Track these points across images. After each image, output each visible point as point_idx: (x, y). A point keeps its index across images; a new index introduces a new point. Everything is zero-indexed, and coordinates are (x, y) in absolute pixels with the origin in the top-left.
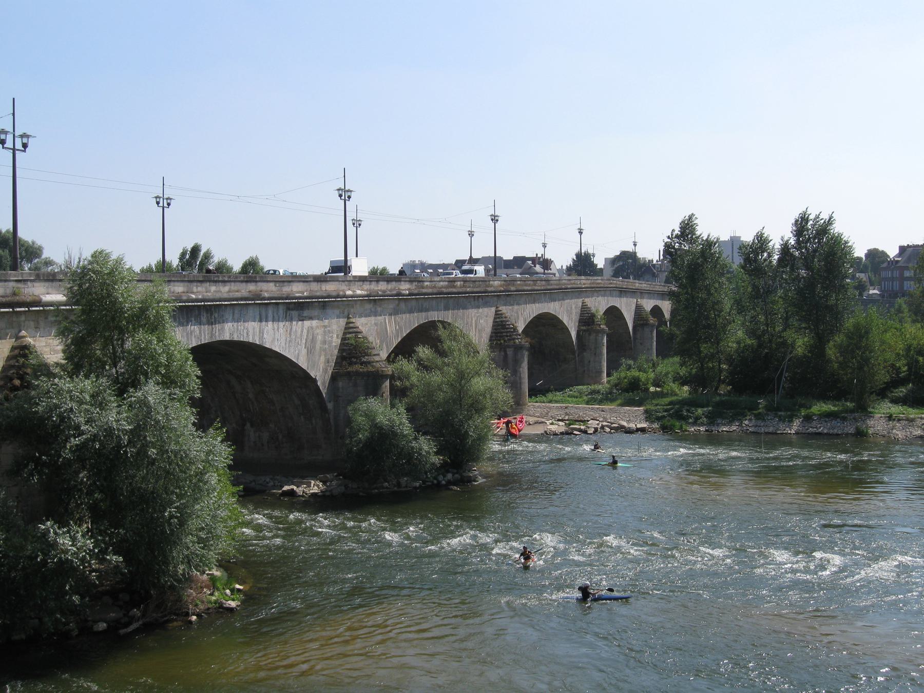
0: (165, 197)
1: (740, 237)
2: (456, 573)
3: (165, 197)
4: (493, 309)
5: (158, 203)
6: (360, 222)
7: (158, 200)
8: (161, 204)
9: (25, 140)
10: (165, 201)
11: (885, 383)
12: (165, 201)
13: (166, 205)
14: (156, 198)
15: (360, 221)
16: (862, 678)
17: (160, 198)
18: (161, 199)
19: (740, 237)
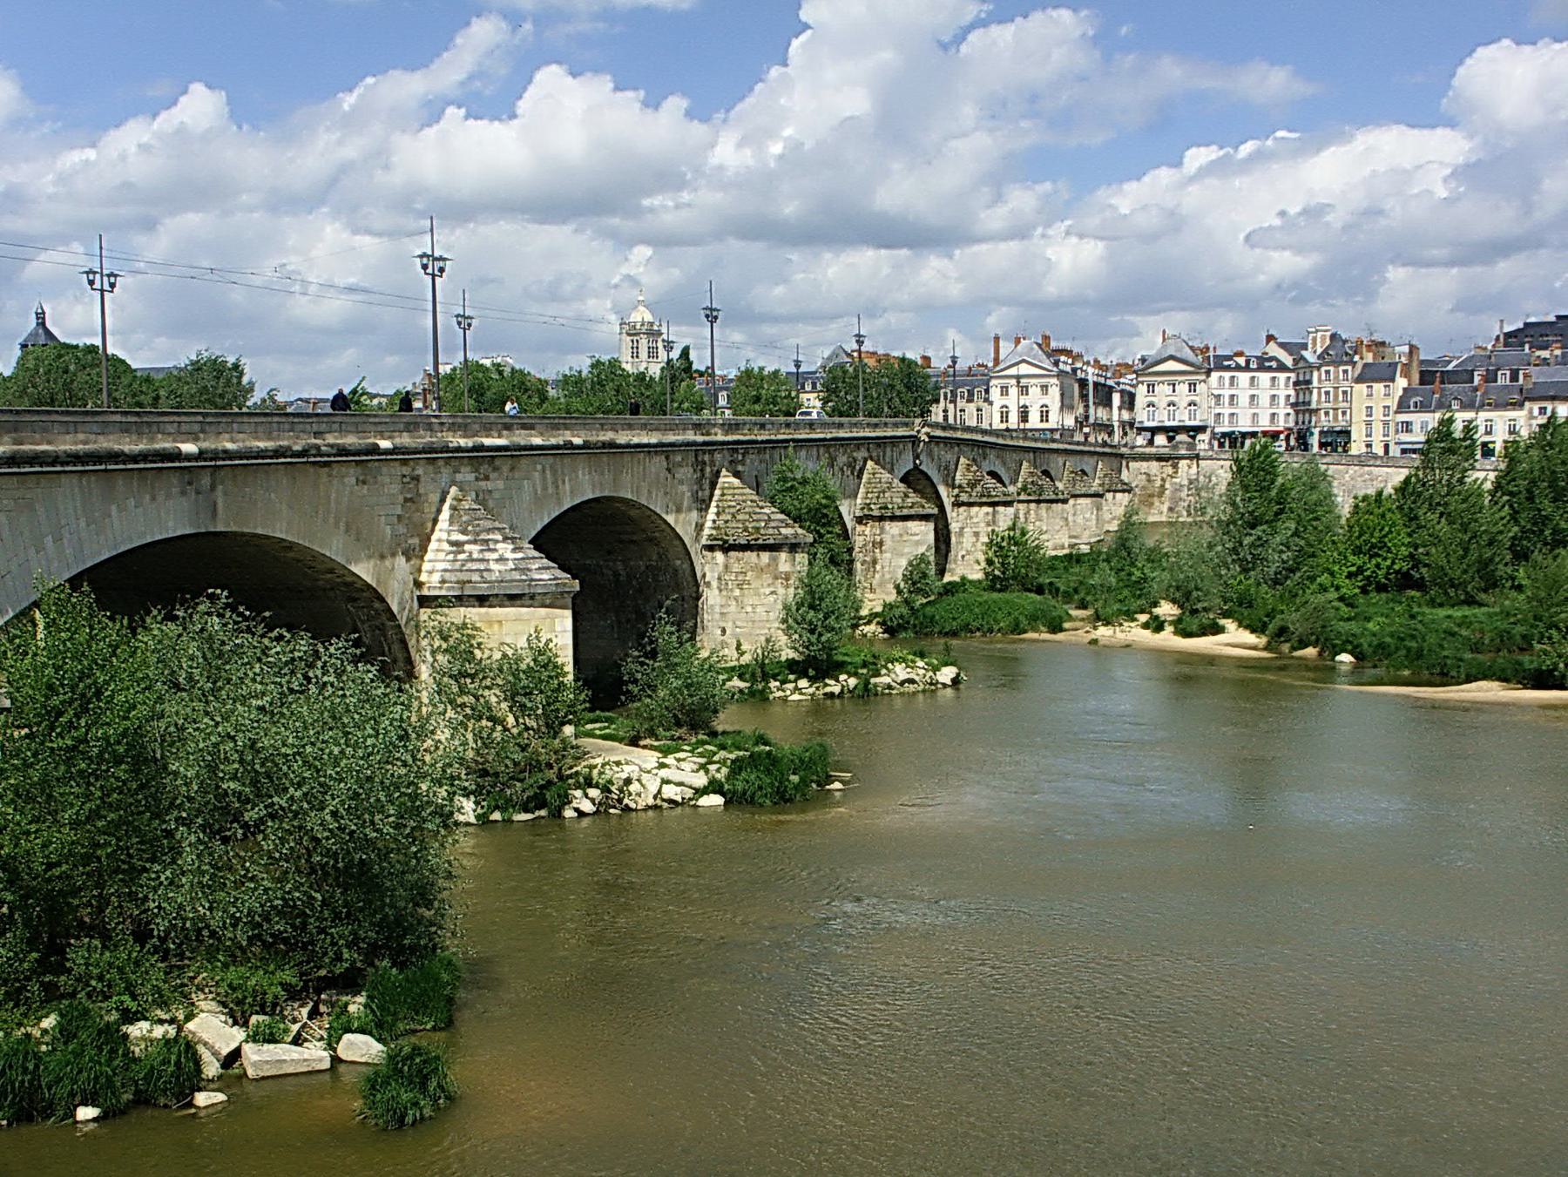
0: (105, 272)
1: (617, 88)
2: (913, 898)
3: (105, 272)
4: (801, 370)
5: (91, 283)
6: (441, 264)
7: (91, 277)
8: (97, 285)
9: (112, 280)
10: (105, 279)
11: (240, 127)
12: (105, 279)
13: (106, 287)
14: (87, 273)
15: (441, 259)
16: (151, 629)
17: (95, 273)
18: (98, 276)
19: (617, 88)
